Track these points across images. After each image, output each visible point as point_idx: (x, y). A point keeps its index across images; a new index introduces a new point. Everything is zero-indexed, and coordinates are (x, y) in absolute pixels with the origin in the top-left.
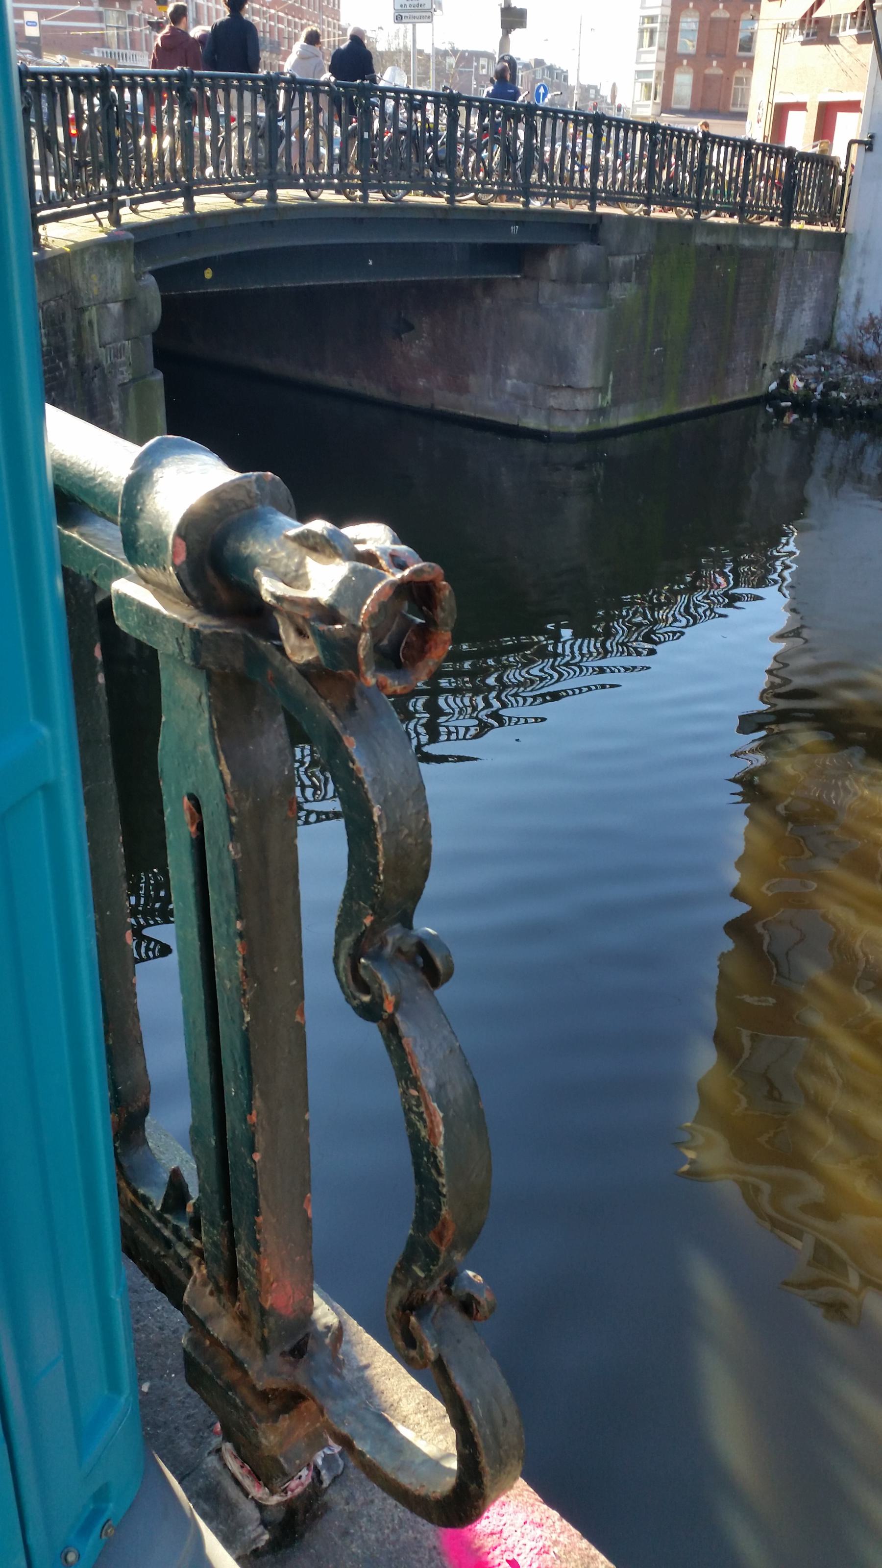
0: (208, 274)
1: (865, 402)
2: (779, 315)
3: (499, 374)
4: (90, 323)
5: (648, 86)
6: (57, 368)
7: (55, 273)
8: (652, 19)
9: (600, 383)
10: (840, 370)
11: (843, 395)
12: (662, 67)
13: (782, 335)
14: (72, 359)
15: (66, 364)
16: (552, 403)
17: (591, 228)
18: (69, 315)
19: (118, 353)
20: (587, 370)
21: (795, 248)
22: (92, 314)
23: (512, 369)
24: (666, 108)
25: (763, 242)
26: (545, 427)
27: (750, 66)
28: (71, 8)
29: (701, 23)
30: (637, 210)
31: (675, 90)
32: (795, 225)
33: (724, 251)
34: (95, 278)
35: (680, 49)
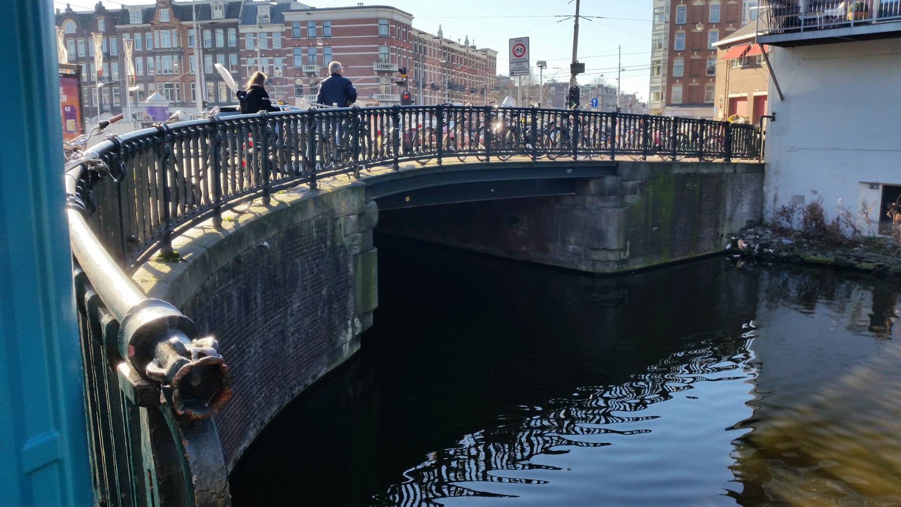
0: (408, 199)
1: (785, 254)
2: (728, 208)
3: (564, 243)
4: (340, 225)
5: (658, 94)
6: (321, 248)
7: (323, 202)
8: (658, 62)
9: (621, 246)
10: (769, 237)
11: (771, 251)
12: (665, 84)
13: (731, 219)
14: (329, 243)
15: (326, 246)
16: (595, 257)
17: (613, 168)
18: (329, 221)
19: (354, 239)
20: (613, 239)
21: (735, 172)
22: (342, 221)
23: (572, 240)
24: (669, 104)
25: (715, 170)
26: (591, 270)
27: (714, 81)
28: (363, 77)
29: (685, 62)
30: (639, 158)
31: (673, 95)
32: (734, 160)
33: (690, 176)
34: (343, 203)
35: (675, 75)
